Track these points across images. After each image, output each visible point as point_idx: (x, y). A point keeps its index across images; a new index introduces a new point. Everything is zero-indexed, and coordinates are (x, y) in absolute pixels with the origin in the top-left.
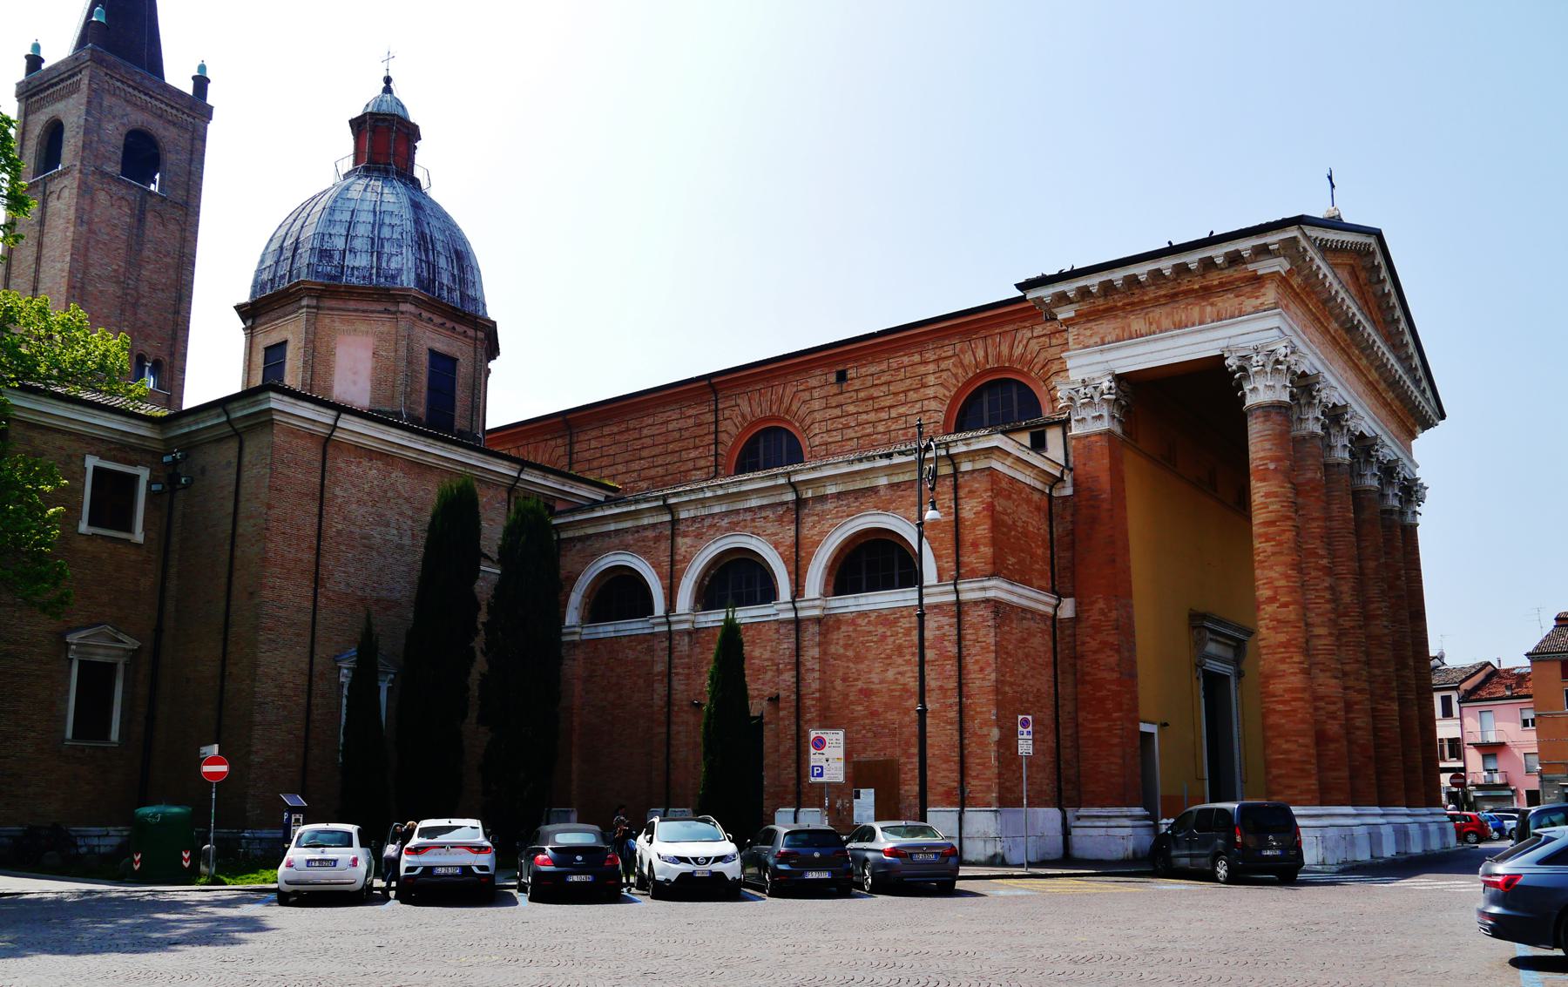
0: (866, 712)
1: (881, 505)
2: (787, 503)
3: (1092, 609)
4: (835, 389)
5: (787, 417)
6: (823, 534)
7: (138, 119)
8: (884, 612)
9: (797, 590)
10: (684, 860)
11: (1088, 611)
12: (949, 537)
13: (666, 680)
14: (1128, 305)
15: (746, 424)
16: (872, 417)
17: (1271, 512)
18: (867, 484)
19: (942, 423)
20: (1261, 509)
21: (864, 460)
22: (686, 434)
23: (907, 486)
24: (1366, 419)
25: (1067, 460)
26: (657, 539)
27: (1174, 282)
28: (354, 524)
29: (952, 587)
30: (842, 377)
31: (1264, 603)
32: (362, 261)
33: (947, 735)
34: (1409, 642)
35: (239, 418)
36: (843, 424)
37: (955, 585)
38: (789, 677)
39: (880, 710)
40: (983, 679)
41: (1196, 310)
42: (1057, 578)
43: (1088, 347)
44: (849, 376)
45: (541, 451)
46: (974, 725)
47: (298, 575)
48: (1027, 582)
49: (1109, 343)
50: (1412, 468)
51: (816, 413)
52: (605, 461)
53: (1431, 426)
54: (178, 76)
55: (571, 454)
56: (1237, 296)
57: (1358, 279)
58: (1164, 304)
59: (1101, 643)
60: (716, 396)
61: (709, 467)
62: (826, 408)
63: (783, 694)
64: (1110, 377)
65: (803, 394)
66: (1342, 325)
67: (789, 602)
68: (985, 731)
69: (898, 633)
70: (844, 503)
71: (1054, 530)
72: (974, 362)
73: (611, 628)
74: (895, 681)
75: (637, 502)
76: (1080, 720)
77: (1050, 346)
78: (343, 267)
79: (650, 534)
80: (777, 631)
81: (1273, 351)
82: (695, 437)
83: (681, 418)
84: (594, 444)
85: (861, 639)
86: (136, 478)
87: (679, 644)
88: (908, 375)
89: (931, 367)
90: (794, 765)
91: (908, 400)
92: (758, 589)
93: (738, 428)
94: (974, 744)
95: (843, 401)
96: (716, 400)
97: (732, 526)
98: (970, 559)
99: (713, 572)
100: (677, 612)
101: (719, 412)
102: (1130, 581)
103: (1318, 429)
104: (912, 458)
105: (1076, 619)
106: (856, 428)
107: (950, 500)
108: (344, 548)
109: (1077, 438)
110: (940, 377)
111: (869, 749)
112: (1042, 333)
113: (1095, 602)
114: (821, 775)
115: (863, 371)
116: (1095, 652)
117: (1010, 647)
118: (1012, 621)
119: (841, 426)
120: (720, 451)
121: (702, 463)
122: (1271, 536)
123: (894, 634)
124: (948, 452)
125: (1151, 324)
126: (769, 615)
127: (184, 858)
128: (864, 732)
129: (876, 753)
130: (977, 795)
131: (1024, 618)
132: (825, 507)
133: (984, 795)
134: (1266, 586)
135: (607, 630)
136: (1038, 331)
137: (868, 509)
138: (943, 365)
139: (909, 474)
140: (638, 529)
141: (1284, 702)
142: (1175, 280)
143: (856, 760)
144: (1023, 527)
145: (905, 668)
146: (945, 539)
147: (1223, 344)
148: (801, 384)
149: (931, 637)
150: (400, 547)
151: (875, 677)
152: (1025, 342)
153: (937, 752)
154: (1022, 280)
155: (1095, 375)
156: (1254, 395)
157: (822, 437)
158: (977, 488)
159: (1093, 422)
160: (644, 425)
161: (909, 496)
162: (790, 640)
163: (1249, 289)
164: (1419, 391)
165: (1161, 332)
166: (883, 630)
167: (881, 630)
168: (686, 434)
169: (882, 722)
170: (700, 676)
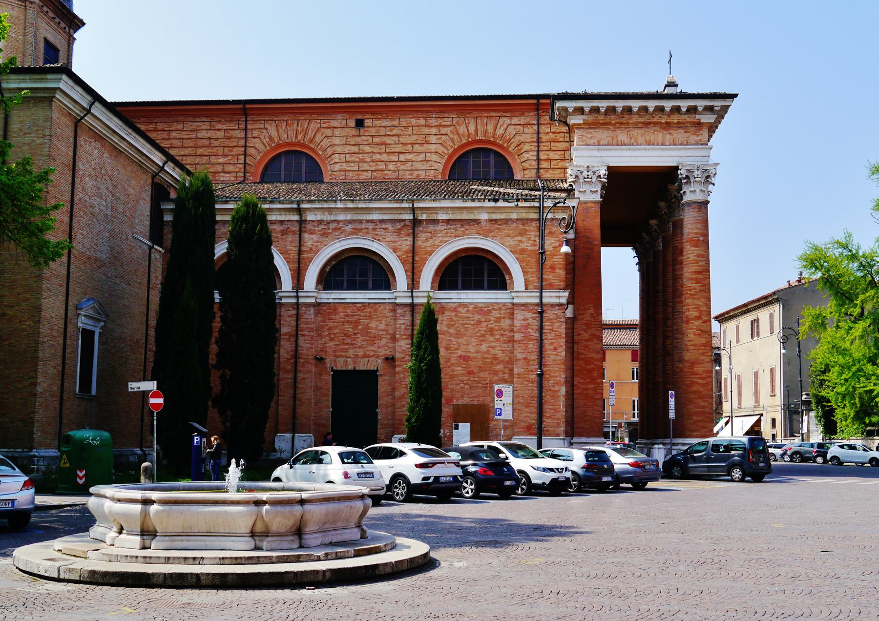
0: (464, 372)
1: (482, 233)
3: (585, 313)
4: (354, 132)
5: (311, 145)
8: (480, 305)
10: (551, 470)
11: (582, 314)
13: (293, 339)
14: (618, 123)
15: (273, 145)
16: (384, 157)
17: (700, 266)
18: (471, 217)
19: (441, 171)
20: (692, 263)
21: (476, 201)
23: (503, 222)
30: (360, 124)
31: (693, 319)
33: (528, 390)
35: (10, 89)
36: (360, 159)
39: (476, 371)
40: (556, 355)
44: (366, 125)
46: (548, 384)
49: (603, 145)
51: (336, 147)
56: (685, 132)
58: (640, 128)
59: (590, 335)
60: (246, 119)
61: (237, 172)
62: (346, 144)
63: (398, 355)
64: (606, 168)
65: (326, 130)
68: (557, 388)
69: (490, 320)
70: (452, 227)
72: (467, 133)
74: (488, 352)
77: (523, 133)
81: (706, 170)
82: (224, 147)
83: (210, 130)
85: (462, 322)
87: (305, 313)
88: (415, 132)
89: (434, 131)
91: (414, 150)
92: (345, 279)
93: (266, 147)
94: (548, 397)
95: (361, 142)
97: (356, 231)
98: (548, 276)
99: (334, 263)
100: (305, 290)
101: (248, 131)
106: (371, 164)
107: (535, 236)
110: (441, 138)
111: (466, 396)
112: (518, 123)
113: (588, 309)
114: (500, 414)
115: (378, 123)
116: (586, 341)
120: (248, 161)
121: (230, 168)
122: (700, 281)
123: (487, 320)
125: (631, 138)
126: (385, 299)
127: (78, 476)
128: (462, 385)
129: (471, 399)
130: (550, 429)
132: (436, 228)
133: (555, 429)
134: (695, 310)
136: (515, 120)
137: (471, 234)
138: (443, 131)
139: (504, 214)
141: (703, 378)
142: (652, 114)
145: (495, 344)
146: (531, 261)
147: (677, 159)
148: (324, 123)
149: (518, 325)
150: (106, 216)
151: (472, 349)
152: (505, 126)
153: (521, 401)
155: (596, 164)
156: (692, 195)
157: (341, 165)
158: (556, 231)
160: (173, 128)
161: (504, 229)
162: (405, 318)
163: (693, 129)
166: (479, 317)
167: (477, 317)
168: (216, 143)
169: (477, 379)
170: (321, 338)
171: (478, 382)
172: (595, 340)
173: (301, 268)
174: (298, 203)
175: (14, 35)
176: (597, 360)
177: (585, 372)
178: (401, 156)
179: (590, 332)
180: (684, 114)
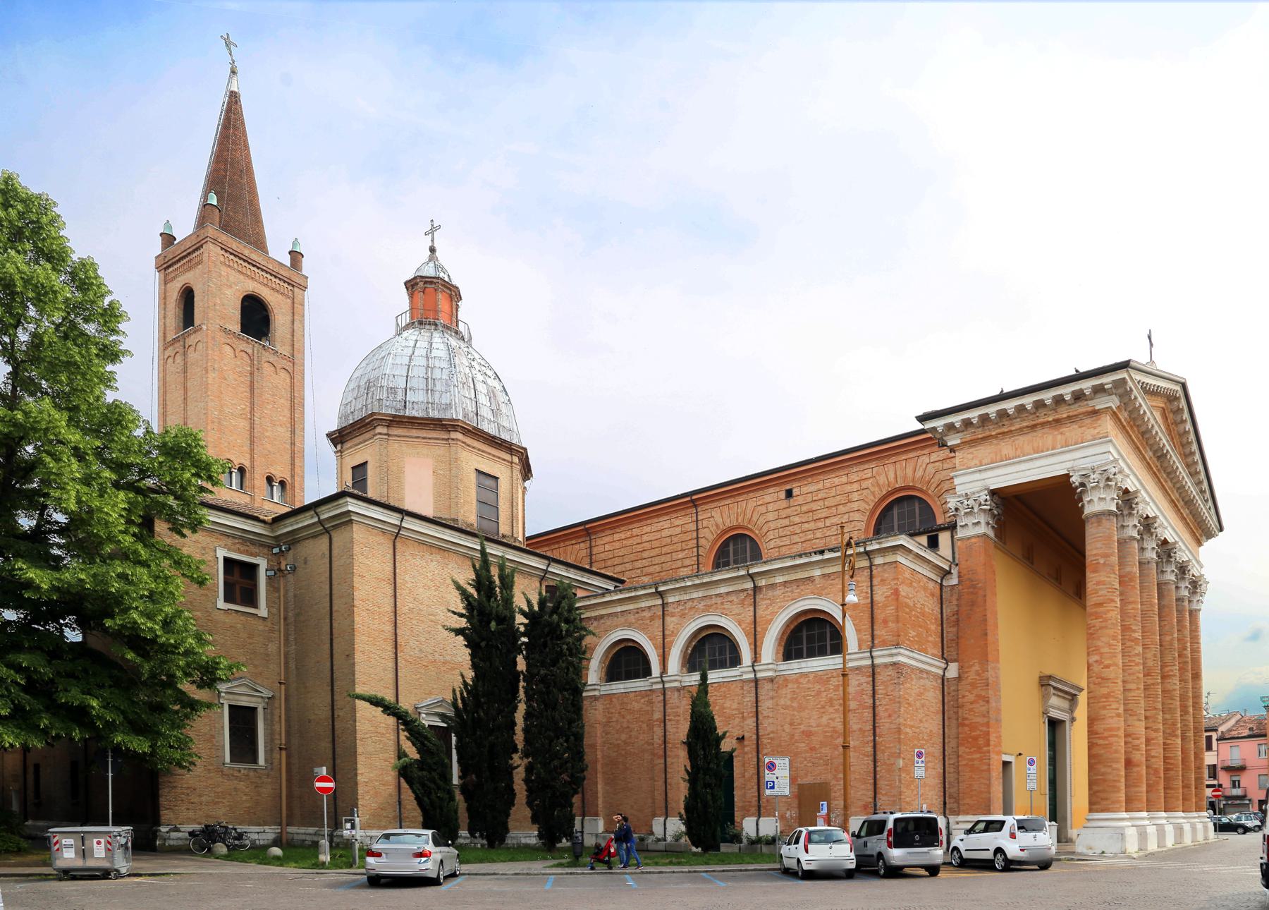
1: (816, 591)
2: (746, 590)
4: (784, 504)
6: (774, 614)
7: (252, 287)
8: (820, 673)
9: (756, 657)
11: (967, 672)
12: (867, 615)
13: (662, 725)
16: (812, 526)
18: (806, 575)
22: (675, 539)
24: (1171, 528)
25: (954, 558)
26: (652, 619)
27: (1034, 416)
28: (422, 604)
29: (869, 654)
30: (789, 494)
32: (420, 397)
34: (1191, 695)
37: (871, 652)
38: (751, 722)
39: (817, 746)
40: (891, 723)
41: (1050, 438)
42: (945, 647)
43: (970, 468)
45: (569, 553)
47: (382, 642)
48: (924, 651)
50: (1199, 569)
52: (616, 561)
53: (1213, 536)
54: (279, 253)
55: (591, 555)
56: (1080, 427)
57: (1167, 419)
63: (746, 735)
64: (986, 492)
65: (760, 507)
66: (1155, 452)
67: (750, 666)
71: (944, 611)
73: (621, 686)
75: (636, 589)
76: (960, 753)
78: (405, 403)
79: (647, 614)
80: (742, 688)
81: (1105, 471)
84: (608, 547)
86: (257, 565)
88: (838, 493)
89: (855, 487)
90: (756, 787)
95: (791, 514)
96: (697, 513)
102: (998, 650)
103: (1135, 534)
104: (839, 554)
105: (959, 678)
108: (415, 622)
109: (960, 539)
112: (937, 459)
115: (805, 490)
116: (972, 703)
117: (910, 699)
118: (912, 680)
119: (789, 533)
120: (700, 553)
124: (865, 548)
125: (1016, 449)
131: (921, 678)
135: (619, 687)
136: (934, 457)
138: (865, 484)
140: (638, 611)
142: (1035, 413)
143: (800, 783)
144: (921, 608)
147: (1069, 465)
149: (854, 692)
151: (813, 723)
153: (857, 777)
154: (920, 413)
159: (976, 527)
164: (1206, 509)
165: (1024, 456)
167: (817, 687)
168: (675, 539)
171: (820, 759)
172: (980, 701)
173: (666, 653)
174: (656, 585)
175: (442, 472)
176: (983, 725)
177: (970, 740)
178: (827, 520)
179: (975, 692)
180: (1092, 399)
